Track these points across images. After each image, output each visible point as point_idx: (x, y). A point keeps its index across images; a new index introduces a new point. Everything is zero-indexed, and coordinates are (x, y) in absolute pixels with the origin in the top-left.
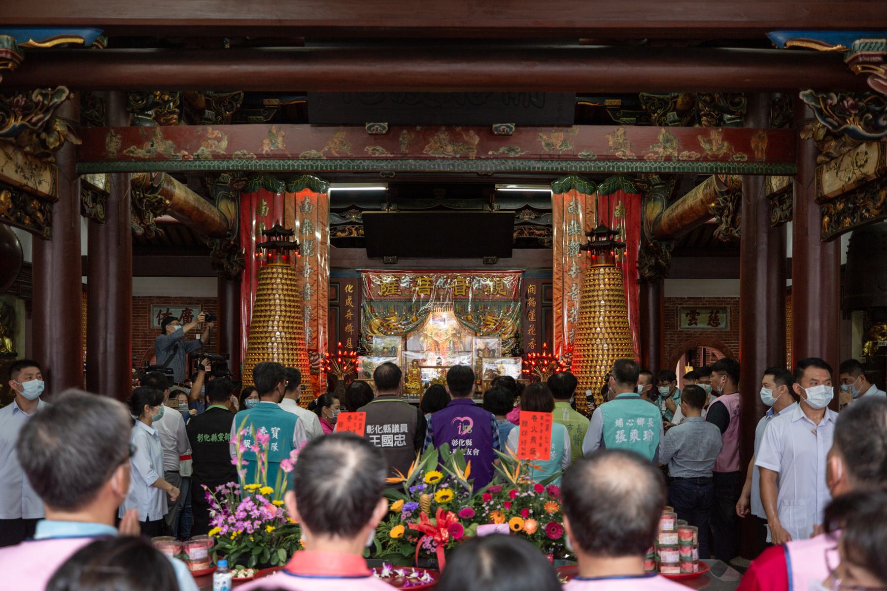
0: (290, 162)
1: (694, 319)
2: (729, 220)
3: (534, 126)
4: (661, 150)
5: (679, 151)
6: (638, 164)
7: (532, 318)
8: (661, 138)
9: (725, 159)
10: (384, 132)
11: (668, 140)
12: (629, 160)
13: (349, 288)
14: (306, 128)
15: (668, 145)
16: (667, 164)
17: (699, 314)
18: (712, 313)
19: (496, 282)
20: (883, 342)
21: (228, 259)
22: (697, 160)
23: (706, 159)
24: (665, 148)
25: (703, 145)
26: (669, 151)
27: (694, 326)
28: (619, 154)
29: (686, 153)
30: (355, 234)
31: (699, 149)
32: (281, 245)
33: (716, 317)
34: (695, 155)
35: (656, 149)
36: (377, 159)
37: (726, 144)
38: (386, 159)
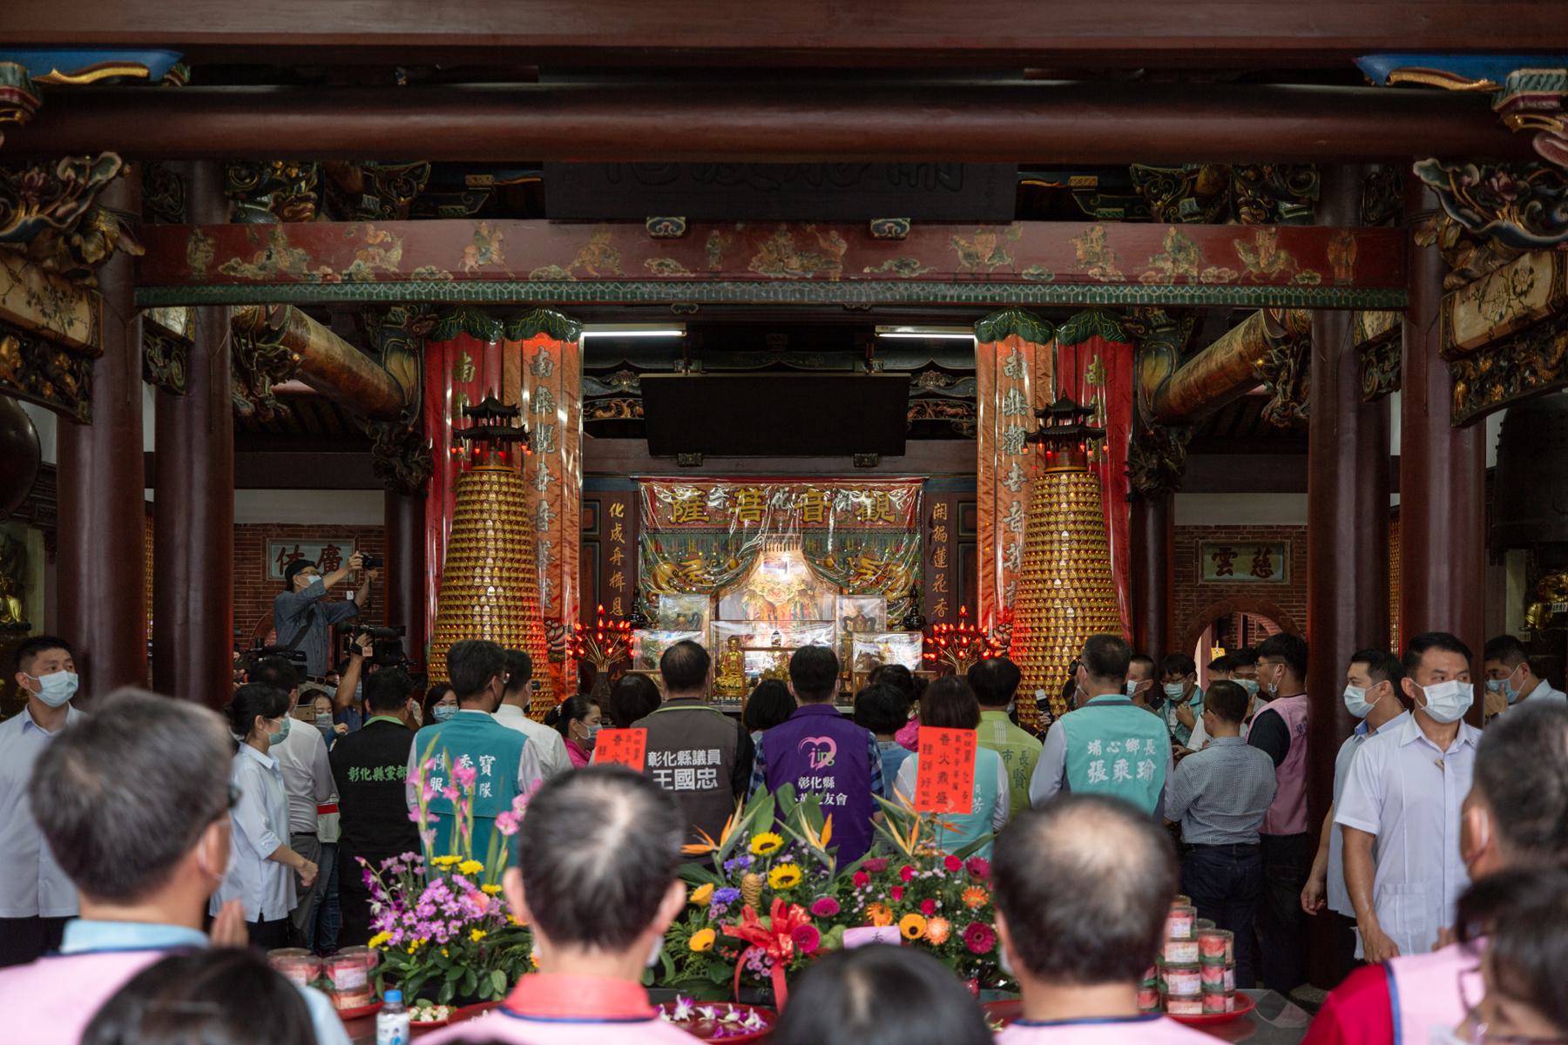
0: (513, 287)
1: (1226, 563)
2: (1289, 388)
3: (944, 222)
4: (1168, 266)
5: (1201, 267)
6: (1128, 290)
7: (940, 562)
8: (1168, 243)
9: (1281, 281)
10: (679, 233)
11: (1180, 248)
12: (1111, 283)
13: (617, 509)
14: (541, 226)
15: (1181, 256)
16: (1178, 291)
17: (1235, 555)
18: (1258, 553)
19: (876, 499)
20: (1561, 604)
21: (404, 457)
22: (1233, 283)
23: (1247, 282)
24: (1175, 261)
25: (1242, 256)
26: (1183, 267)
27: (1227, 576)
28: (1094, 272)
29: (1212, 270)
30: (627, 414)
31: (1236, 263)
32: (498, 432)
33: (1266, 560)
34: (1229, 274)
35: (1160, 264)
36: (667, 281)
37: (1283, 255)
38: (683, 281)
